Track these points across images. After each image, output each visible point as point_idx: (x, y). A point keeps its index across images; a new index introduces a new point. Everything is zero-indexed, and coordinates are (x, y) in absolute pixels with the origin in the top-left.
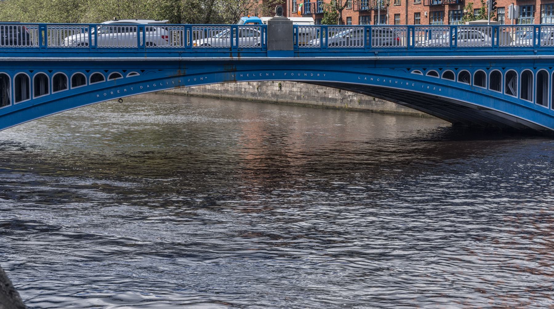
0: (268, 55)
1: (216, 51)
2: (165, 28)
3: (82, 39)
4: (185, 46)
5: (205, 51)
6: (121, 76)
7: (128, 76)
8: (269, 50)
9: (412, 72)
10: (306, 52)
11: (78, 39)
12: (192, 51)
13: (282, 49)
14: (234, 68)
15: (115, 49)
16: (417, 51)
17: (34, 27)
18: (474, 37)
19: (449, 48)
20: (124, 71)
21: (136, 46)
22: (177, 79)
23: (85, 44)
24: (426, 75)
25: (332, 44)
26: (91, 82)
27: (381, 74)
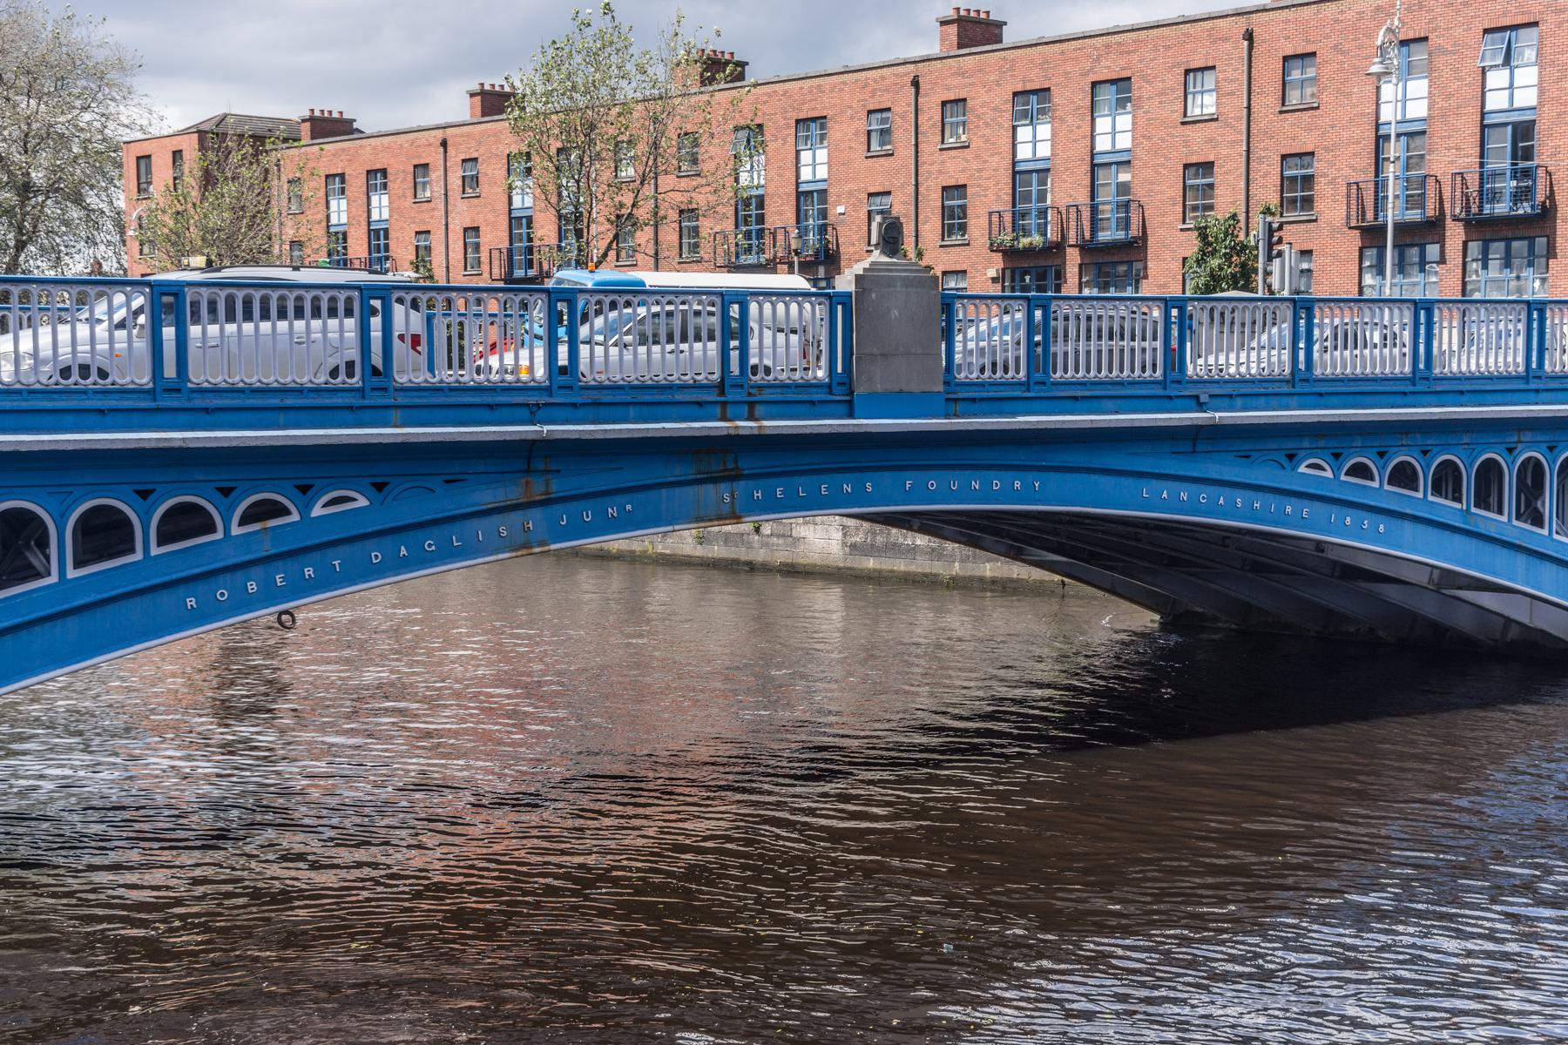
0: (857, 409)
1: (670, 398)
2: (408, 297)
3: (83, 348)
4: (154, 378)
5: (628, 399)
6: (287, 512)
7: (317, 511)
8: (860, 390)
9: (1302, 469)
10: (982, 399)
11: (65, 350)
12: (579, 400)
13: (905, 389)
14: (730, 465)
15: (265, 391)
16: (1323, 390)
17: (1518, 307)
18: (704, 334)
19: (151, 393)
20: (304, 489)
21: (145, 380)
22: (516, 517)
23: (94, 371)
24: (236, 531)
25: (342, 370)
26: (160, 544)
27: (1213, 475)
